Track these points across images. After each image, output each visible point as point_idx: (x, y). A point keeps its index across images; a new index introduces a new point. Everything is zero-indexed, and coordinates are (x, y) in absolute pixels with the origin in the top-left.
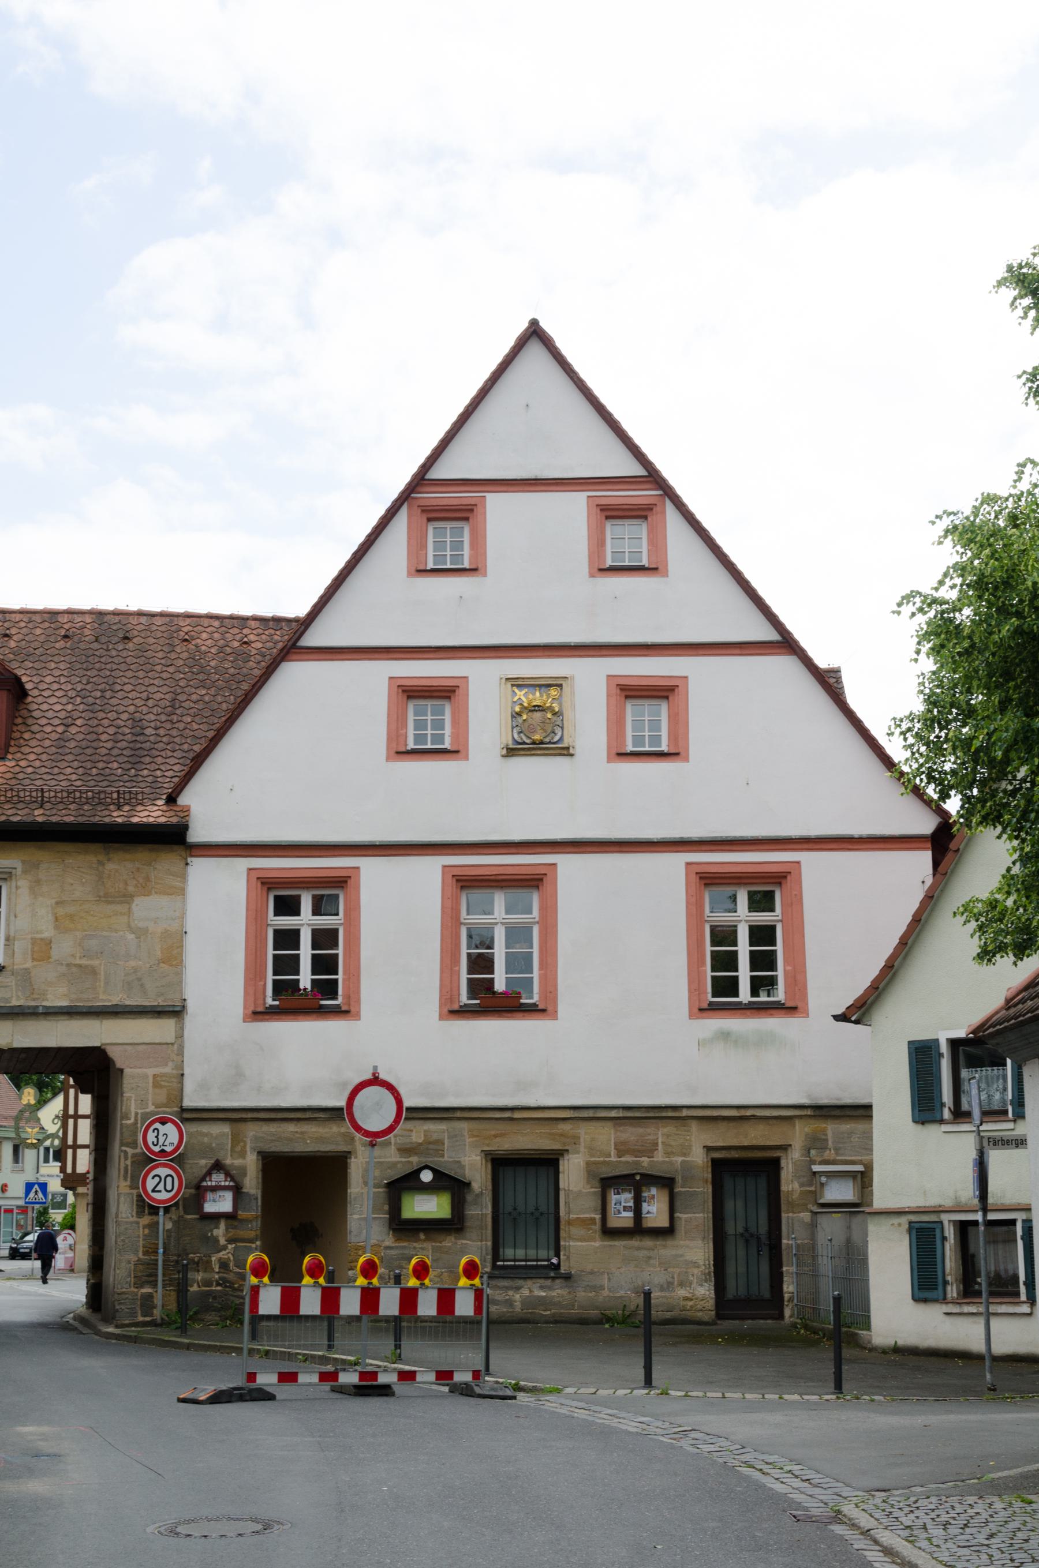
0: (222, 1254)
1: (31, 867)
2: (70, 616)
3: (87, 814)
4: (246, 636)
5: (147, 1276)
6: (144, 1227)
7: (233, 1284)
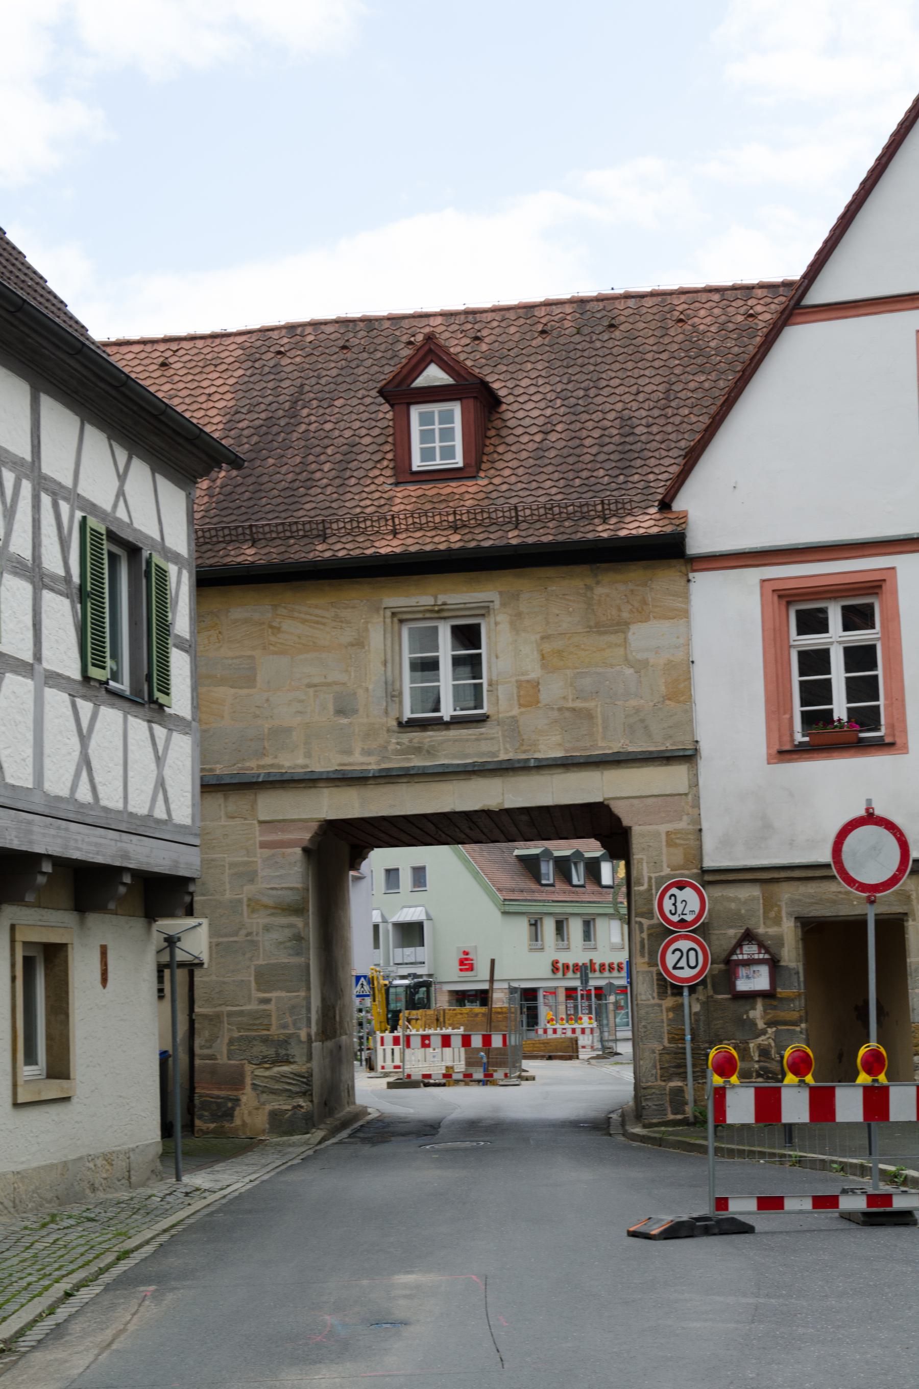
0: (761, 1040)
1: (511, 598)
2: (548, 308)
3: (568, 531)
4: (752, 308)
5: (675, 1067)
6: (668, 1010)
7: (777, 1075)
